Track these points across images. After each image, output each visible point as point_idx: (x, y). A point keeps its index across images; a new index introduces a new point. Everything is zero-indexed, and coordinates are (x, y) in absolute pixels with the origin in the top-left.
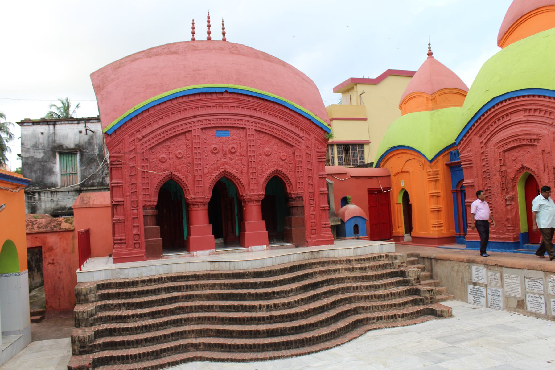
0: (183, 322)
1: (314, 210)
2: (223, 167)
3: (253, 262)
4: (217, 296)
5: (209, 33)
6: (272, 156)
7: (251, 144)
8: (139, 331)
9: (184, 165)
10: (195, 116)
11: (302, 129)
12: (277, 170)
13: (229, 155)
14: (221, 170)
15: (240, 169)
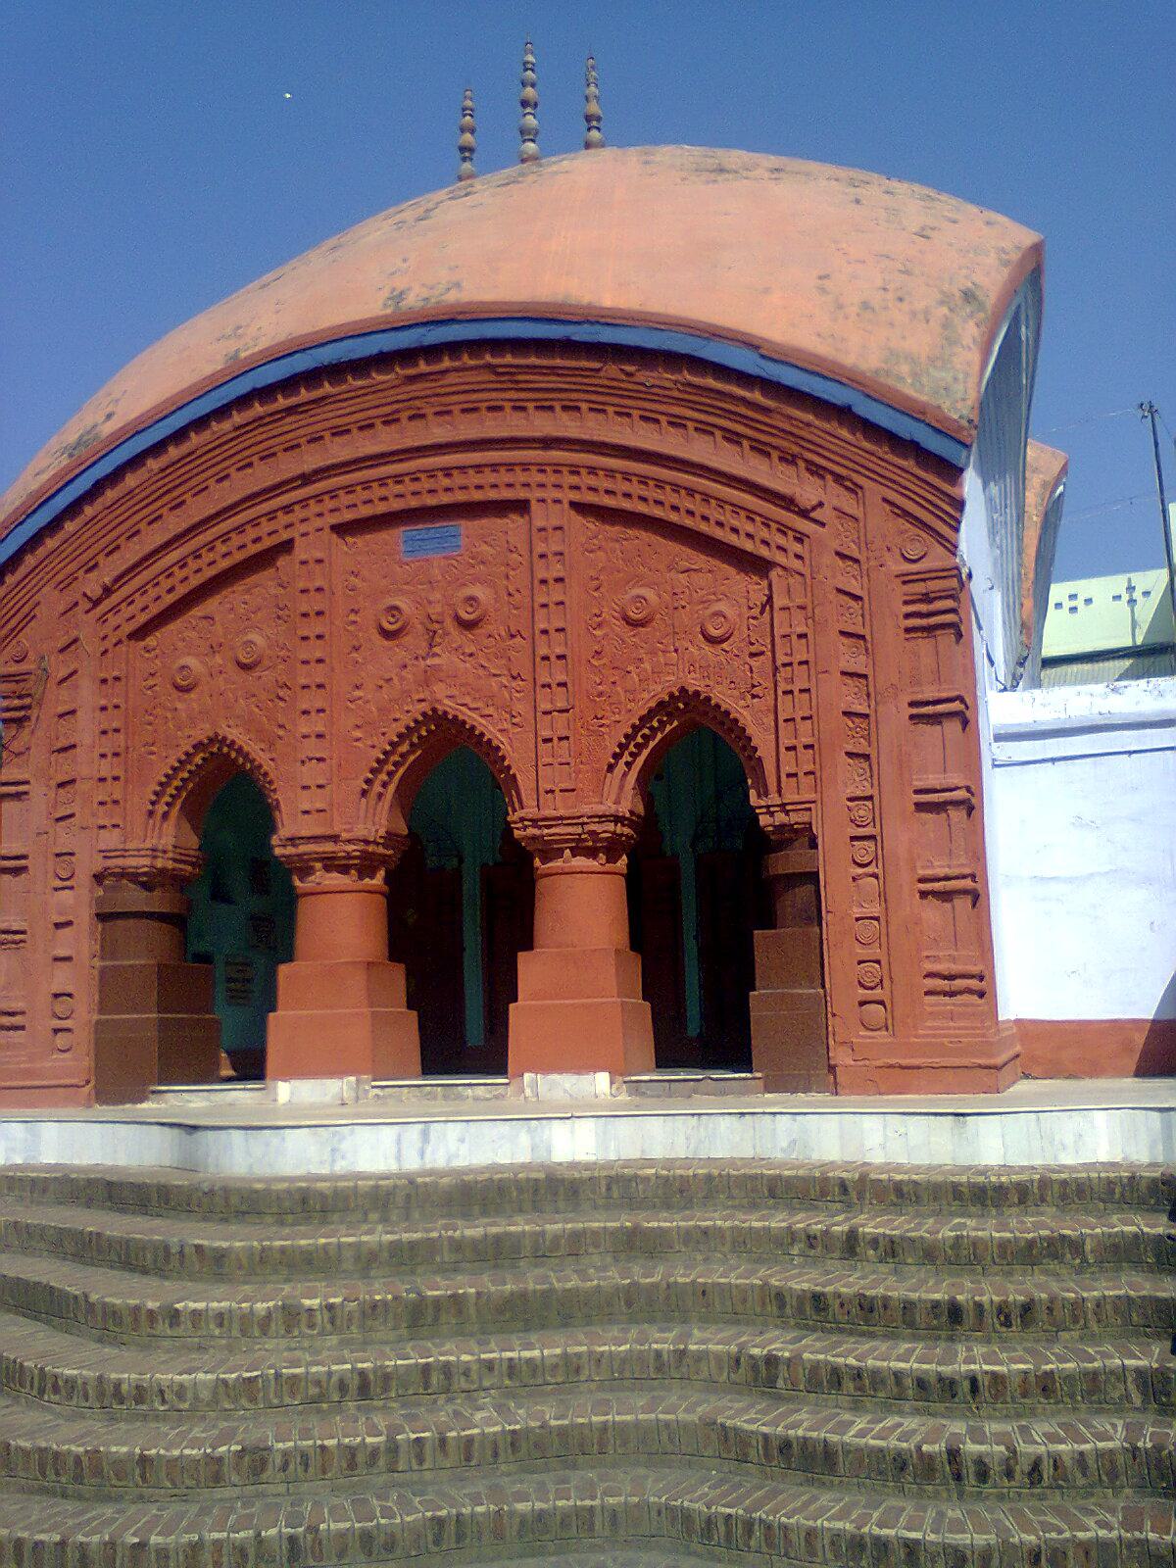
7: (550, 575)
10: (306, 479)
11: (816, 470)
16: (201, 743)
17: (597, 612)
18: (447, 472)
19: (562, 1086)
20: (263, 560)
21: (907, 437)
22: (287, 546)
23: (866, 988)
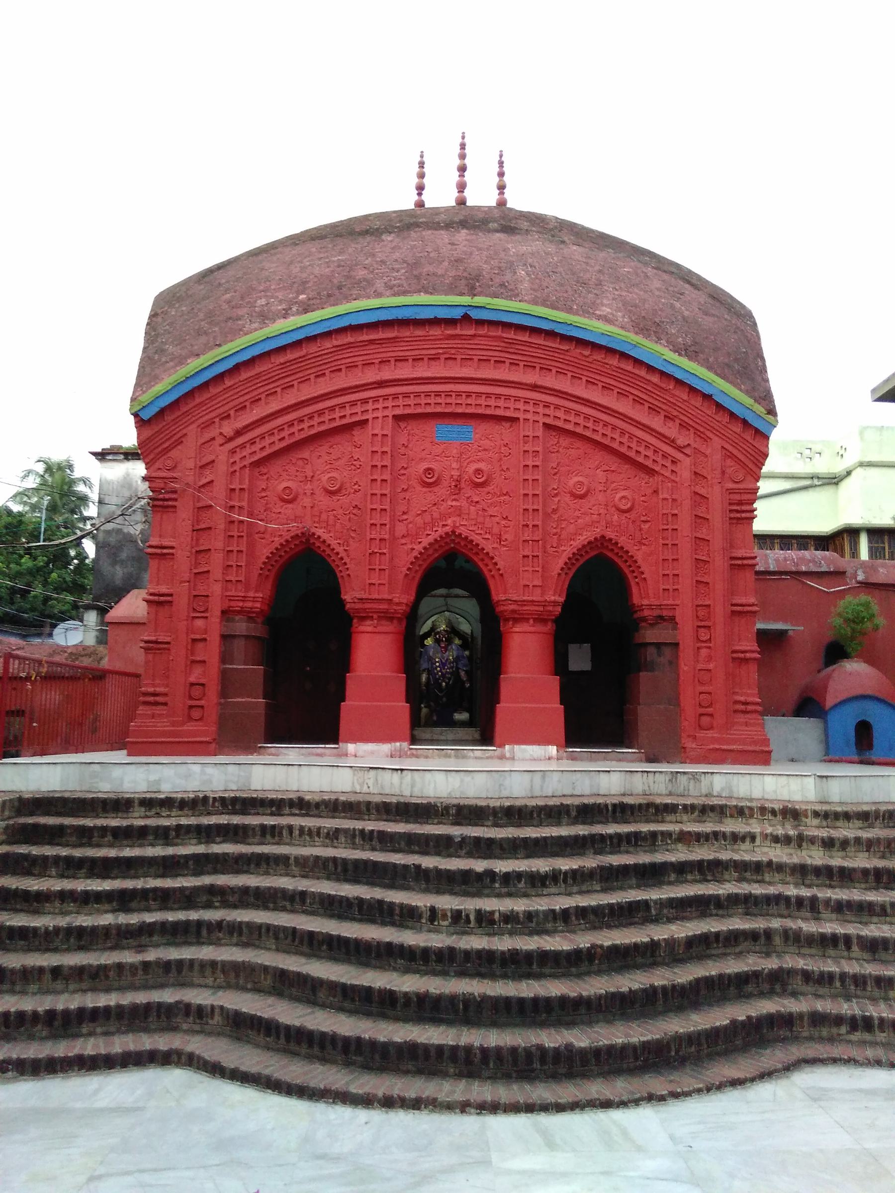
0: (204, 932)
1: (710, 659)
2: (449, 522)
3: (468, 778)
4: (331, 866)
5: (462, 187)
8: (57, 942)
9: (341, 511)
11: (683, 426)
12: (603, 537)
13: (468, 492)
14: (441, 531)
15: (496, 530)
18: (469, 395)
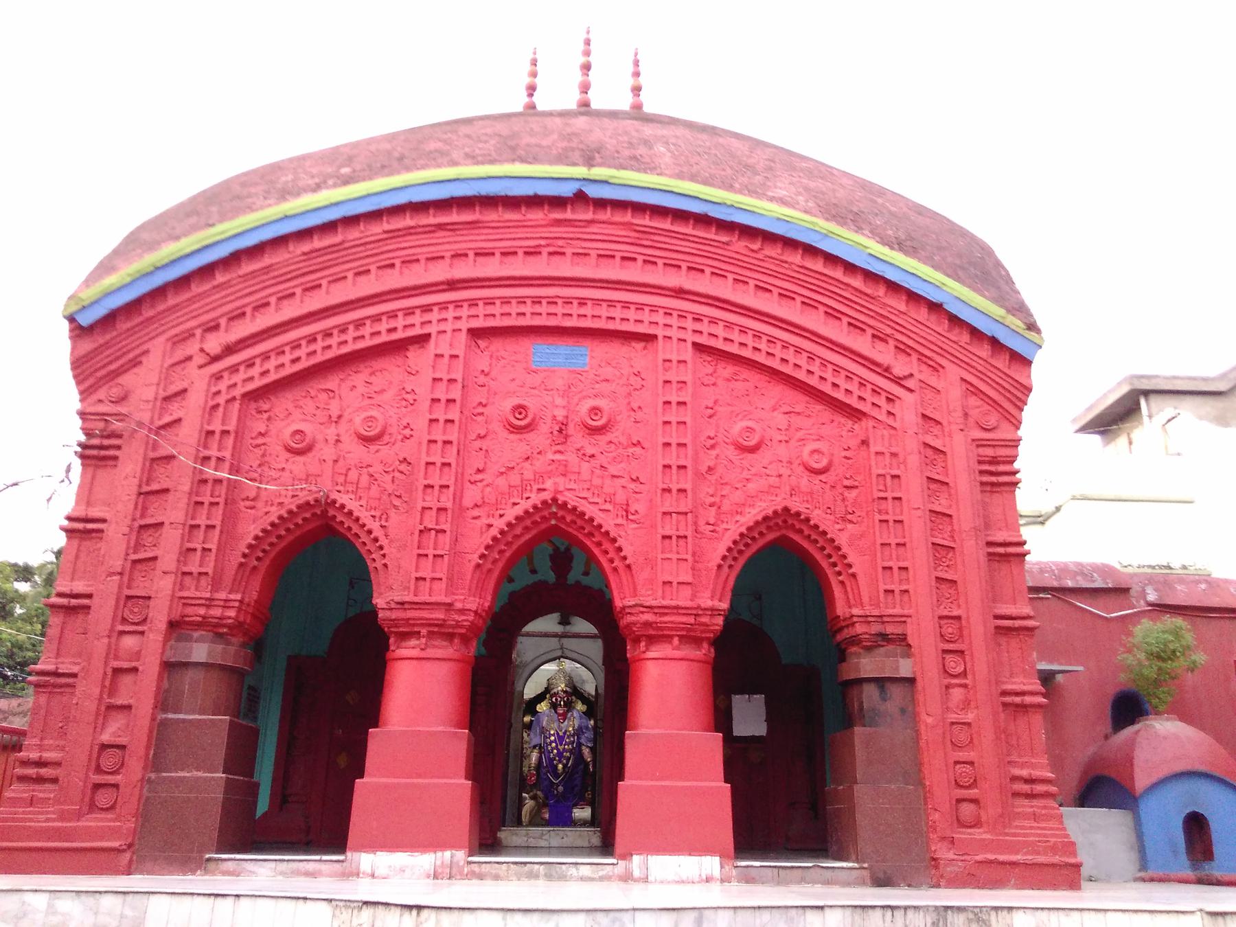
1: (966, 704)
6: (764, 457)
11: (902, 349)
13: (578, 439)
16: (308, 503)
17: (712, 435)
19: (663, 866)
20: (398, 347)
21: (989, 334)
22: (423, 339)
23: (962, 787)
